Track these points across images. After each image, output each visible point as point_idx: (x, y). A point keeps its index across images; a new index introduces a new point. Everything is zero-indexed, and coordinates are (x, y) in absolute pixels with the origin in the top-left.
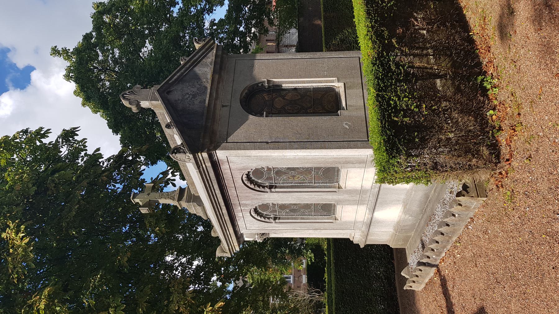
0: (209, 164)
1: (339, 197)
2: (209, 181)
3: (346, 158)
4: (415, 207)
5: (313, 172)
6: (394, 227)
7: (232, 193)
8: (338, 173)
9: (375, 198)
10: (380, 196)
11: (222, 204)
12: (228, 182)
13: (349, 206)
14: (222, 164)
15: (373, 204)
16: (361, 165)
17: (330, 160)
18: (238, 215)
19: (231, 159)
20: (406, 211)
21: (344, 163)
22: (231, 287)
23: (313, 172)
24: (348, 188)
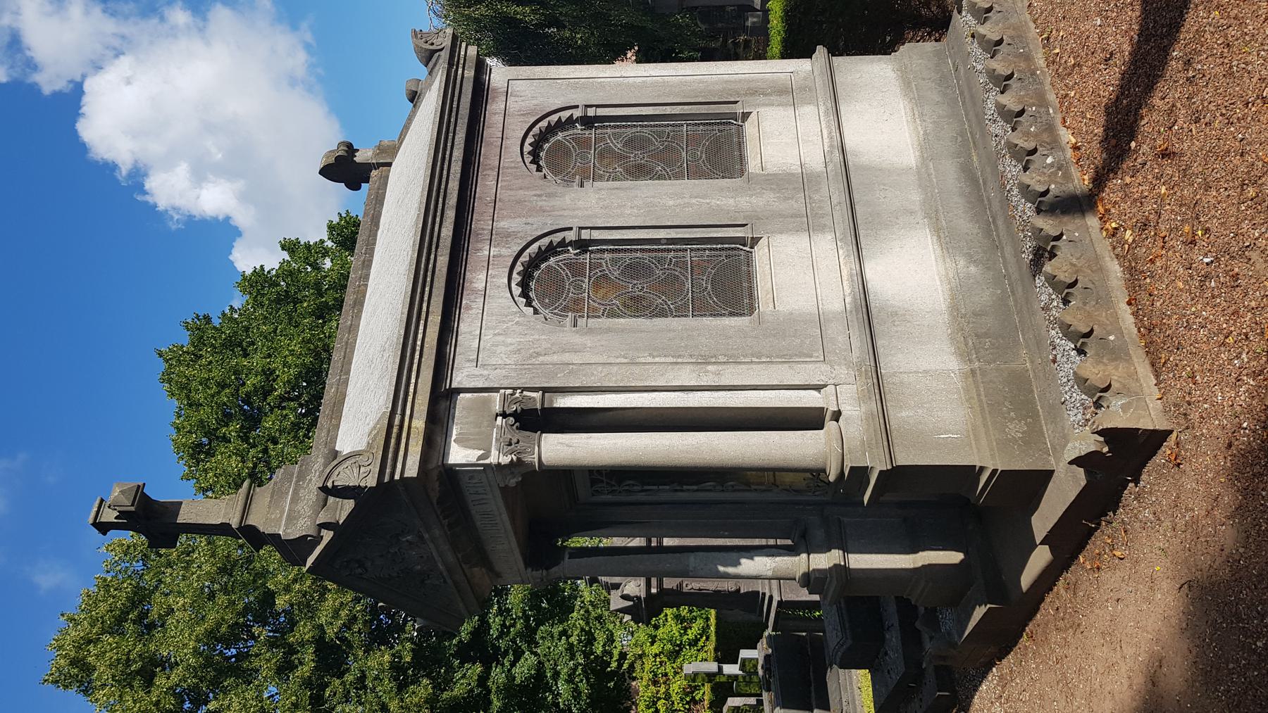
0: (470, 73)
1: (754, 200)
2: (454, 114)
3: (749, 81)
4: (965, 225)
5: (684, 154)
6: (952, 339)
7: (488, 154)
8: (740, 150)
9: (842, 186)
10: (856, 196)
11: (453, 200)
12: (492, 132)
13: (784, 237)
14: (494, 98)
15: (829, 93)
16: (783, 99)
17: (717, 87)
18: (480, 252)
19: (517, 86)
20: (948, 240)
21: (746, 95)
22: (252, 599)
23: (684, 154)
24: (771, 168)
